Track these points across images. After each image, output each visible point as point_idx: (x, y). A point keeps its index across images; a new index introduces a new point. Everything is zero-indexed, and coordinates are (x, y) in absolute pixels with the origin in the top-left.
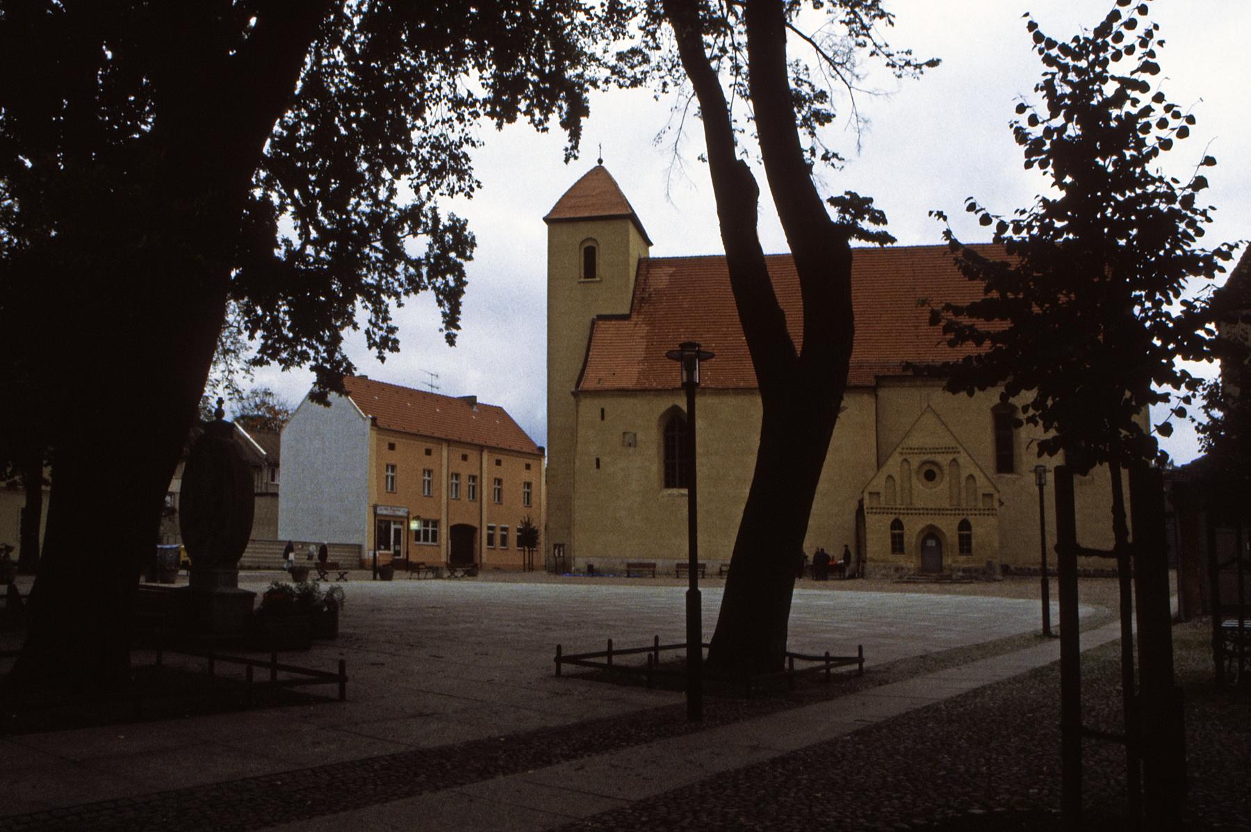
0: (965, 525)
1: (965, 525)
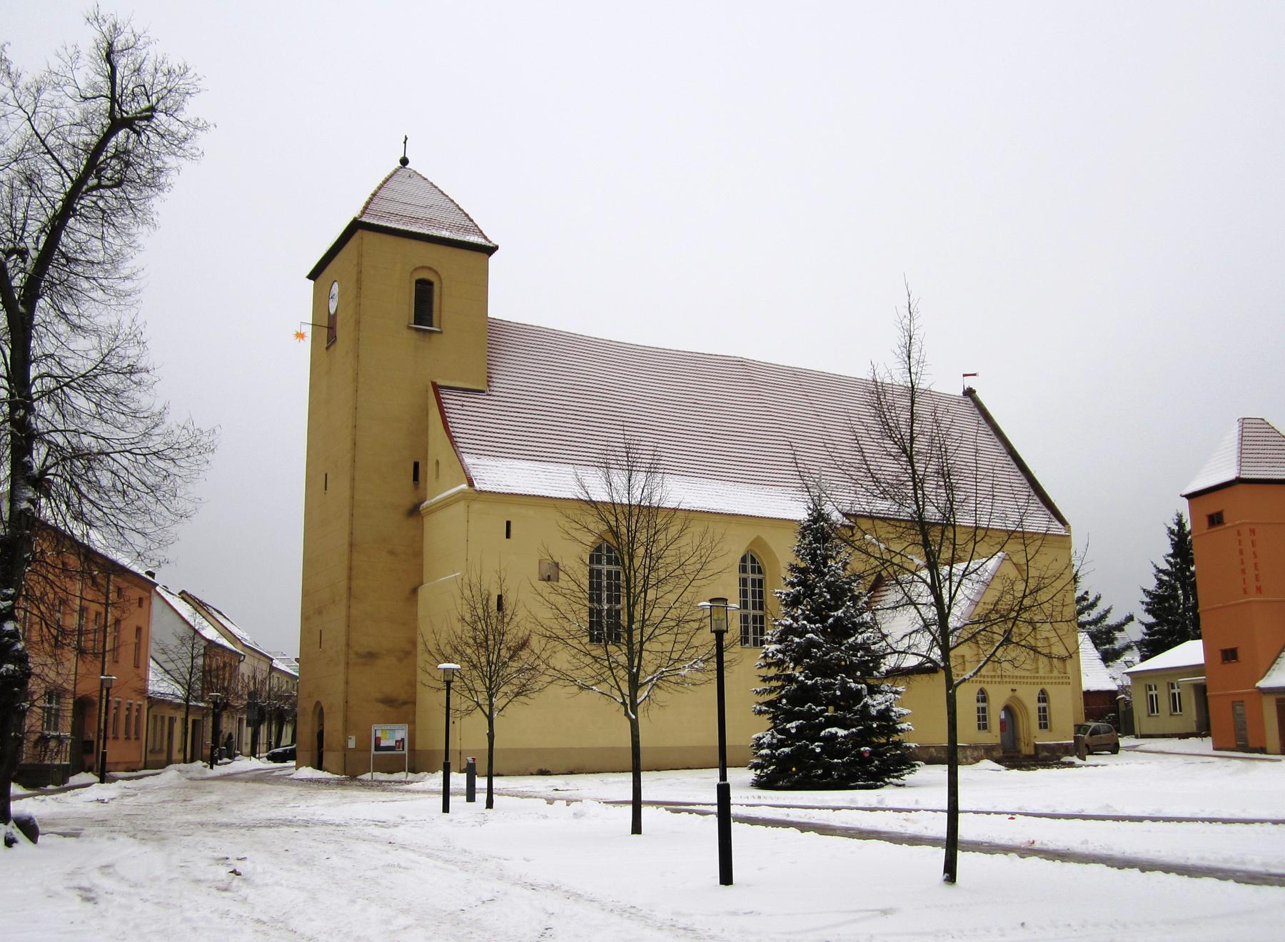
0: (1043, 697)
1: (1043, 697)
